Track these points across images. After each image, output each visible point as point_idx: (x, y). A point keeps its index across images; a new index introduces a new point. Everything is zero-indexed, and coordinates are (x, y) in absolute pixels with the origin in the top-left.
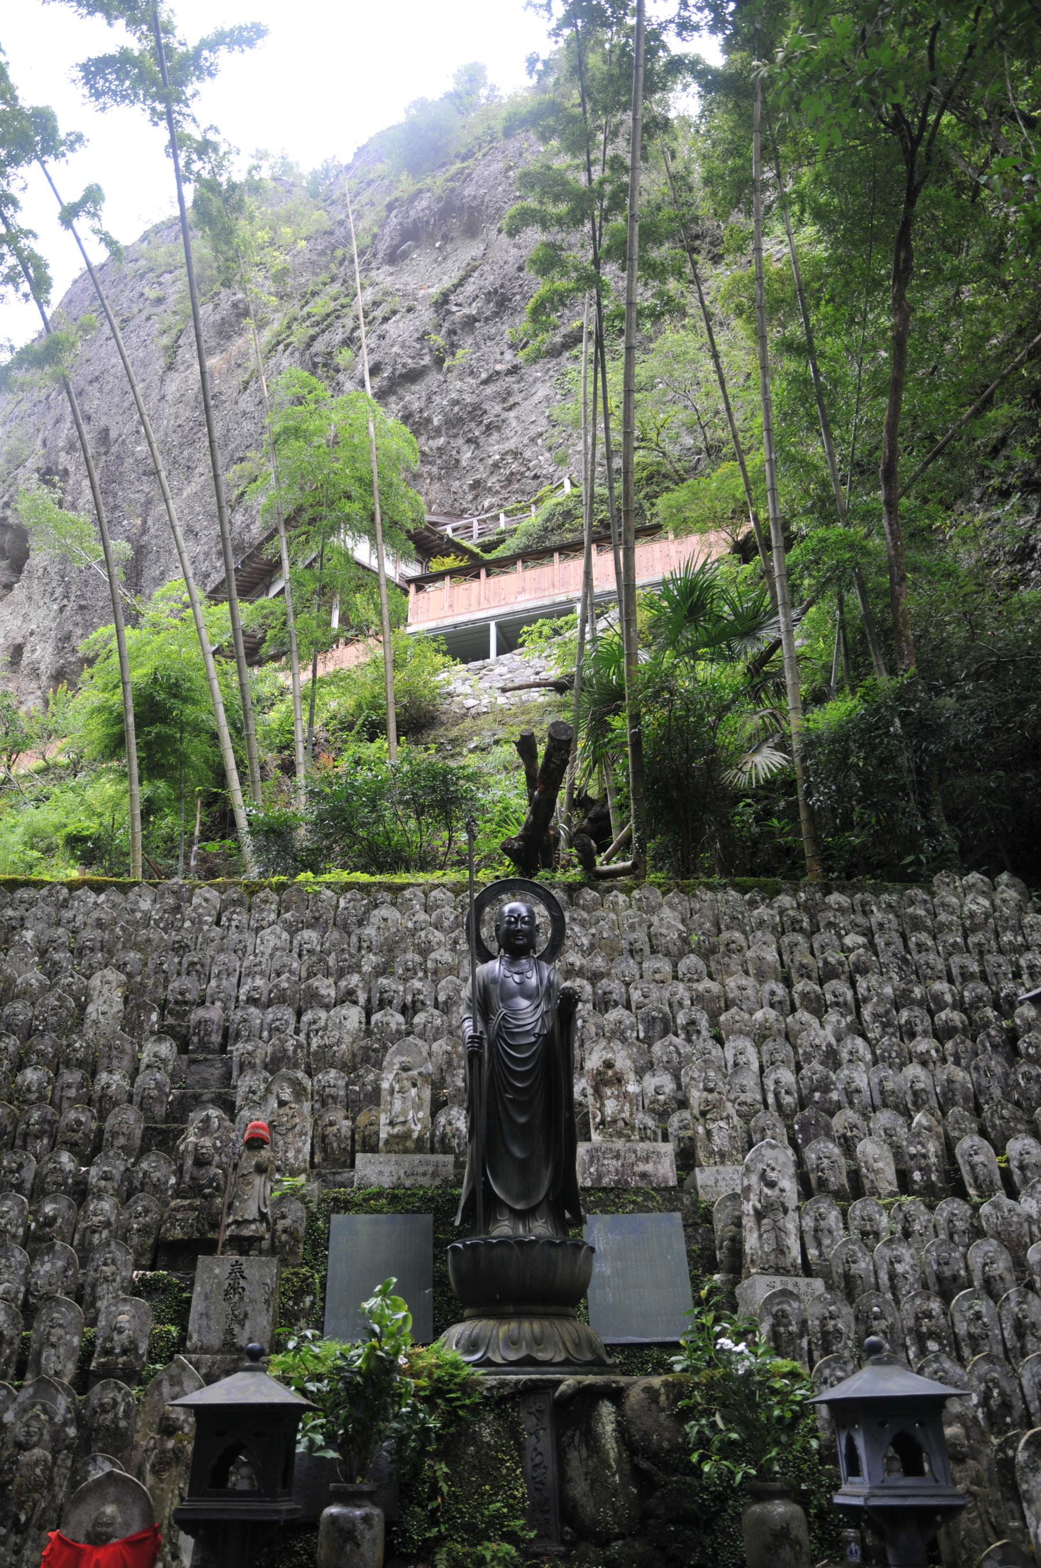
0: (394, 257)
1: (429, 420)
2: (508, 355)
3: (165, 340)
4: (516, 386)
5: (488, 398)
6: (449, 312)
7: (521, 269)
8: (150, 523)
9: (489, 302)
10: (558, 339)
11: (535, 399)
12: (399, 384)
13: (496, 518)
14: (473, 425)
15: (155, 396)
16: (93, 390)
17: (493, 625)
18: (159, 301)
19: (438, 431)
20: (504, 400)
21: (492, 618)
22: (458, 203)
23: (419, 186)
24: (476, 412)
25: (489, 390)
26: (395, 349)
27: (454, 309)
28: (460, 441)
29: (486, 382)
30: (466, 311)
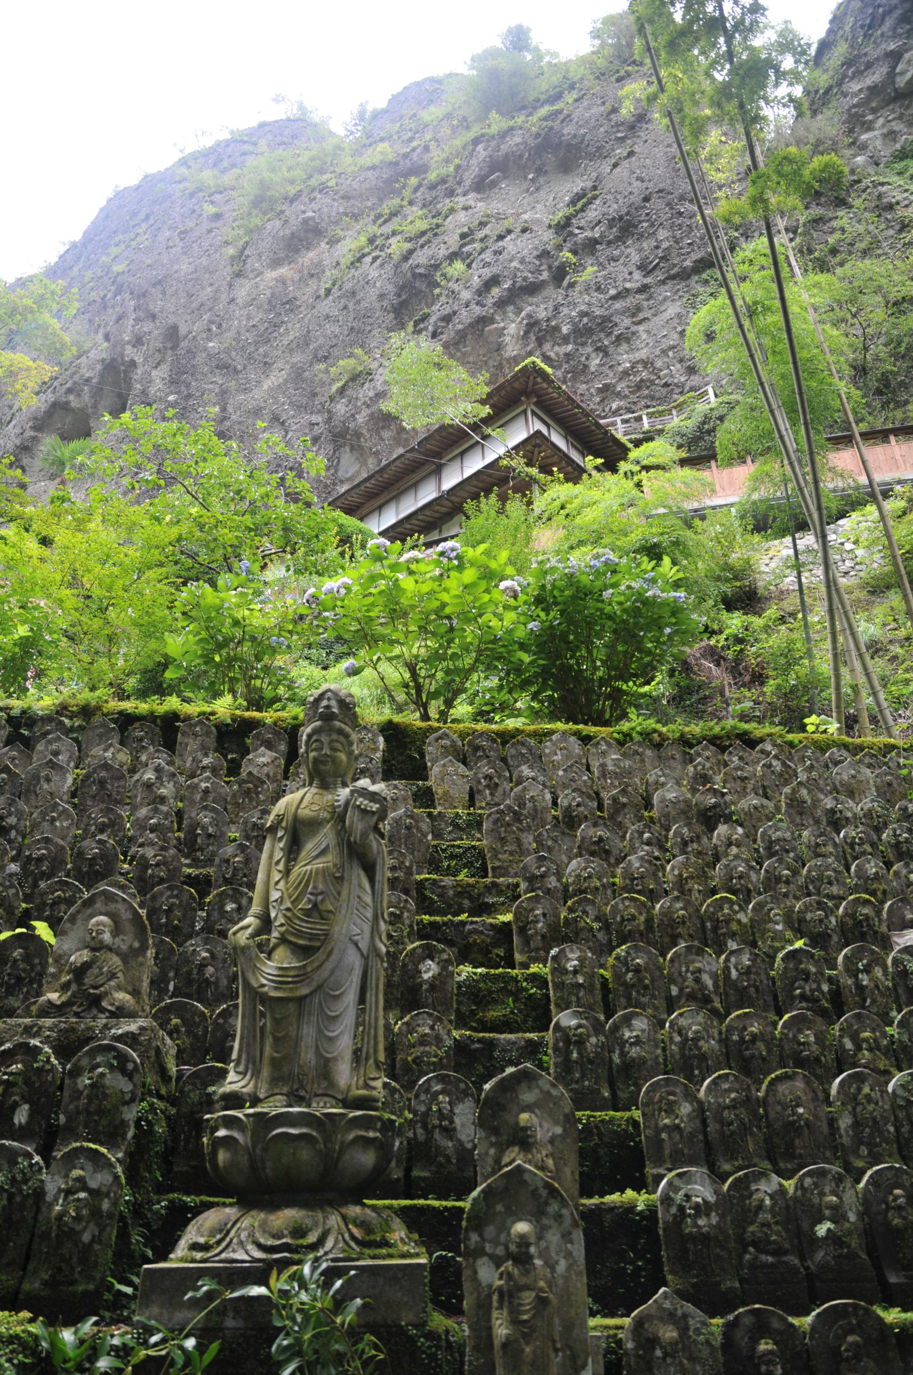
0: (481, 186)
1: (557, 328)
2: (637, 275)
3: (231, 251)
4: (645, 304)
5: (617, 312)
6: (571, 234)
7: (646, 199)
8: (230, 409)
9: (611, 227)
10: (688, 263)
11: (666, 316)
12: (518, 296)
13: (639, 419)
14: (602, 335)
15: (224, 298)
16: (156, 292)
18: (217, 217)
19: (566, 340)
20: (634, 315)
22: (557, 140)
23: (511, 123)
24: (605, 324)
25: (618, 305)
26: (515, 264)
27: (577, 231)
28: (589, 349)
30: (589, 234)
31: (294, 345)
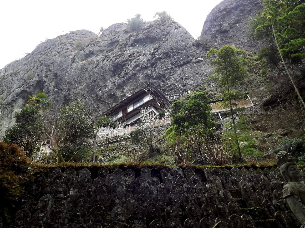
2: (170, 65)
5: (166, 73)
6: (155, 56)
17: (219, 113)
19: (155, 79)
21: (220, 112)
24: (164, 75)
25: (166, 72)
27: (156, 56)
29: (165, 70)
31: (87, 79)
